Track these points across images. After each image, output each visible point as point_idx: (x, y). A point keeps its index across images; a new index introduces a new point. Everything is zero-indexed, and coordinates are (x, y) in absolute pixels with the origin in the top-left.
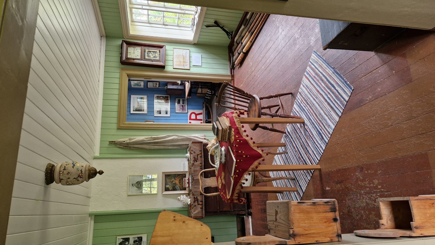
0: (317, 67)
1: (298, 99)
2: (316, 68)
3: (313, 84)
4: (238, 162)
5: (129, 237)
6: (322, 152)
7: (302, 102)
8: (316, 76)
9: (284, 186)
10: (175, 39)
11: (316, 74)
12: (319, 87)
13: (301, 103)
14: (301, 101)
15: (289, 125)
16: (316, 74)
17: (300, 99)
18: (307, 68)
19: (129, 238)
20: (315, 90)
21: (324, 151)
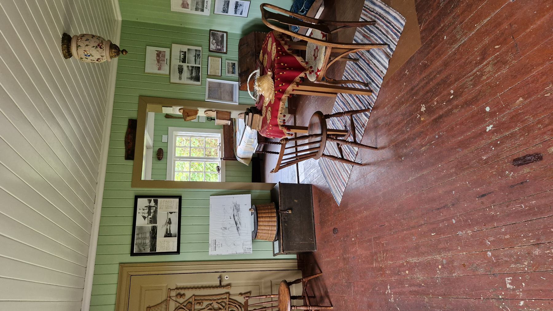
0: (336, 187)
1: (353, 157)
2: (337, 187)
3: (339, 171)
4: (281, 72)
5: (253, 183)
6: (376, 98)
7: (348, 153)
8: (337, 178)
9: (281, 164)
10: (147, 119)
11: (336, 180)
12: (334, 168)
13: (349, 153)
14: (349, 155)
15: (365, 122)
16: (336, 180)
17: (350, 157)
18: (404, 27)
19: (252, 182)
20: (338, 166)
21: (377, 97)
